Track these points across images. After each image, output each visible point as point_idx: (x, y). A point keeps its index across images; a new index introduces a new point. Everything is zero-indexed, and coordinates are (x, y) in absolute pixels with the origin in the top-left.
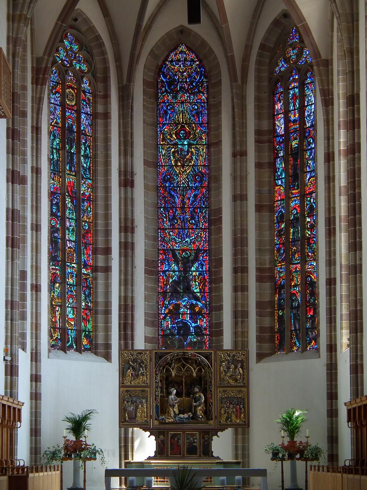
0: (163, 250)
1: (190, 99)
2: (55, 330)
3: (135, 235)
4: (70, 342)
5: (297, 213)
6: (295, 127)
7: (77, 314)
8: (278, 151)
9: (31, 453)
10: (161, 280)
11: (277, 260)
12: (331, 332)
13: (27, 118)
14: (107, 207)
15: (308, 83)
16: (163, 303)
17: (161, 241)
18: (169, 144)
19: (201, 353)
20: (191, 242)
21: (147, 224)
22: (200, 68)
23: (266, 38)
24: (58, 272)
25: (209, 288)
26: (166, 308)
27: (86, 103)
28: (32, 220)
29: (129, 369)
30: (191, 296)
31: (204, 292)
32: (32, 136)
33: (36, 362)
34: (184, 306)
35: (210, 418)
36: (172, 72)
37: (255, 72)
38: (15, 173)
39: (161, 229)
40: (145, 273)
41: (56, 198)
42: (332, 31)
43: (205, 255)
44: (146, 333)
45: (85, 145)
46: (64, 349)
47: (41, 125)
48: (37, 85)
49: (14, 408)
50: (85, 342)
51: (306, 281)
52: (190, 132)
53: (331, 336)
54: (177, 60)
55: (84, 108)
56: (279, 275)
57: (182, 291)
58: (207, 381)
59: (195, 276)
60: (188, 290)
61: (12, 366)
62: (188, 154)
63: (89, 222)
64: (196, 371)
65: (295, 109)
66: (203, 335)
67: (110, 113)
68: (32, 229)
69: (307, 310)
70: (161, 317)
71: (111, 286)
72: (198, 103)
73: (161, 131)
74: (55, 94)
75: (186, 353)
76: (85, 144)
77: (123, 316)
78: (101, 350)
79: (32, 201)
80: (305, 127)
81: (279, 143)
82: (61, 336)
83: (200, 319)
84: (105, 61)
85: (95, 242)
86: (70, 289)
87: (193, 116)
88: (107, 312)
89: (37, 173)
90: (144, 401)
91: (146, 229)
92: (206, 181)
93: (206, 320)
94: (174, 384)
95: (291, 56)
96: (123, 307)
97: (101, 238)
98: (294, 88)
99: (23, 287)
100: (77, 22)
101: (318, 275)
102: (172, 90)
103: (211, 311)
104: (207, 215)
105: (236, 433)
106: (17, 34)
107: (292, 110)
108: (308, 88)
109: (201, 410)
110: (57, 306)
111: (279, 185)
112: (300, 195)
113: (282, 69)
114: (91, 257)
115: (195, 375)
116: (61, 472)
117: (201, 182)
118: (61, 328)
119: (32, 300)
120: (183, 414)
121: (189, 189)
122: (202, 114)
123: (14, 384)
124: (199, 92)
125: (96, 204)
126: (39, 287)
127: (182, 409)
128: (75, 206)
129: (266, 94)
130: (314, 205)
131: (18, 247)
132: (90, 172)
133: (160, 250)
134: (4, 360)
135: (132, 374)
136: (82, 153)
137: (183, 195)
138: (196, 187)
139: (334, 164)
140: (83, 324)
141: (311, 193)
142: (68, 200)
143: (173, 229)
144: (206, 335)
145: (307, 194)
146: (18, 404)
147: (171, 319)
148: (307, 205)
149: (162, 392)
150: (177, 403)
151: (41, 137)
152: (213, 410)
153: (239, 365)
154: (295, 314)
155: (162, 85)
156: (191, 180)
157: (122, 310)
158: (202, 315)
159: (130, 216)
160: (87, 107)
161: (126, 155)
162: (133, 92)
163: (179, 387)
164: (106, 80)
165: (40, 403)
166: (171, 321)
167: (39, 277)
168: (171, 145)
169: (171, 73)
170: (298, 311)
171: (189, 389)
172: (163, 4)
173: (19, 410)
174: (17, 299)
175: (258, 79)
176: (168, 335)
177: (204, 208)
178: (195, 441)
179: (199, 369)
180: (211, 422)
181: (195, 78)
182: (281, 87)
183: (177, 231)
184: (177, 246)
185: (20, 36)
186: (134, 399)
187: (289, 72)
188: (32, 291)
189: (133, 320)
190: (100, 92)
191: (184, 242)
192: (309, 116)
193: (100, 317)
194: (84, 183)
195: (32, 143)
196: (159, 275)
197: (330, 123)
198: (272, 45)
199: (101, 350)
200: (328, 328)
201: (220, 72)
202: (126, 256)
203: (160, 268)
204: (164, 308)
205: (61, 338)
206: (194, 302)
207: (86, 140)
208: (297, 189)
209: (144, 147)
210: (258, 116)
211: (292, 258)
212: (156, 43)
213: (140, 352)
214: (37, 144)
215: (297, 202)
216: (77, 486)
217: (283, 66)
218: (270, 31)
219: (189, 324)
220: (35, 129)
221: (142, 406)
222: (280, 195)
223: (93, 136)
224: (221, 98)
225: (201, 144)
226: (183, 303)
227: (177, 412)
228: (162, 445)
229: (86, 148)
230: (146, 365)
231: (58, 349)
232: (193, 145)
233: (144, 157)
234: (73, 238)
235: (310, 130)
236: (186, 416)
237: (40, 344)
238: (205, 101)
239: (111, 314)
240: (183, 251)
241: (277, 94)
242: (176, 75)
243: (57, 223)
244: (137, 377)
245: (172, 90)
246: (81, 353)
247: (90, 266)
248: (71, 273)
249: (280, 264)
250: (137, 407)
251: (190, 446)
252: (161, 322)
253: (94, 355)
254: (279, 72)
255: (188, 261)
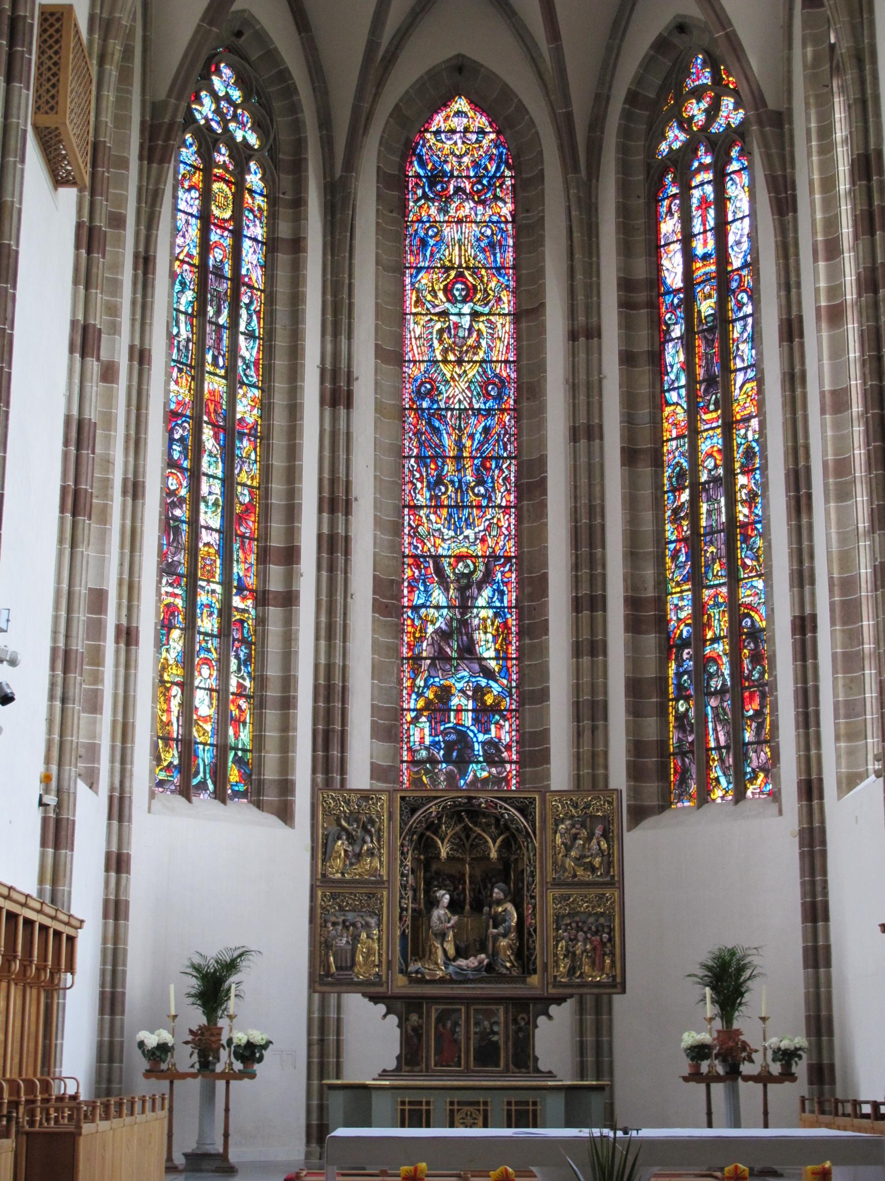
0: (415, 556)
1: (476, 214)
2: (167, 745)
3: (353, 519)
4: (201, 774)
5: (716, 467)
6: (707, 269)
7: (218, 706)
8: (668, 326)
9: (99, 1059)
10: (410, 629)
11: (672, 579)
12: (808, 748)
13: (124, 229)
14: (293, 452)
15: (734, 172)
16: (413, 685)
17: (409, 535)
18: (431, 314)
19: (510, 798)
20: (476, 539)
21: (380, 493)
22: (497, 147)
23: (639, 80)
24: (179, 602)
25: (518, 649)
26: (420, 695)
27: (255, 216)
28: (126, 472)
29: (339, 838)
30: (476, 667)
31: (506, 659)
32: (135, 277)
33: (120, 820)
34: (462, 691)
35: (531, 967)
36: (438, 156)
37: (617, 152)
38: (91, 330)
39: (409, 507)
40: (374, 611)
41: (181, 426)
42: (790, 46)
43: (507, 569)
44: (375, 755)
45: (248, 309)
46: (186, 791)
47: (155, 252)
48: (150, 162)
49: (58, 934)
50: (234, 775)
51: (740, 627)
52: (475, 287)
53: (808, 759)
54: (449, 131)
55: (248, 227)
56: (677, 614)
57: (455, 655)
58: (523, 871)
59: (484, 620)
60: (468, 651)
61: (58, 821)
62: (470, 334)
63: (251, 487)
64: (497, 844)
65: (705, 232)
66: (503, 762)
67: (305, 238)
68: (124, 493)
69: (743, 699)
70: (409, 719)
71: (297, 639)
72: (493, 222)
73: (412, 284)
74: (189, 190)
75: (475, 798)
76: (248, 306)
77: (321, 713)
78: (271, 797)
79: (127, 426)
80: (729, 269)
81: (673, 308)
82: (180, 758)
83: (497, 723)
84: (297, 126)
85: (264, 535)
86: (204, 644)
87: (483, 251)
88: (287, 703)
89: (141, 363)
90: (373, 921)
91: (377, 505)
92: (509, 397)
93: (510, 725)
94: (444, 880)
95: (693, 116)
96: (322, 691)
97: (277, 526)
98: (702, 184)
99: (96, 629)
100: (243, 38)
101: (773, 610)
102: (437, 194)
103: (521, 703)
104: (512, 475)
105: (581, 1009)
106: (111, 12)
107: (699, 234)
108: (734, 183)
109: (510, 947)
110: (173, 683)
111: (674, 404)
112: (723, 422)
113: (676, 146)
114: (254, 569)
115: (494, 855)
116: (171, 1110)
117: (499, 398)
118: (181, 740)
119: (117, 665)
120: (467, 958)
121: (474, 414)
122: (501, 246)
123: (62, 868)
124: (496, 198)
125: (268, 445)
126: (133, 634)
127: (462, 945)
128: (223, 448)
129: (642, 201)
130: (754, 444)
131: (87, 513)
132: (257, 370)
133: (408, 556)
134: (41, 804)
135: (346, 851)
136: (242, 328)
137: (460, 429)
138: (489, 411)
139: (802, 345)
140: (231, 731)
141: (747, 419)
142: (207, 432)
143: (436, 507)
144: (511, 762)
145: (738, 422)
146: (67, 924)
147: (431, 722)
148: (739, 445)
149: (415, 899)
150: (453, 927)
151: (154, 279)
152: (537, 947)
153: (598, 832)
154: (717, 707)
155: (417, 184)
156: (478, 394)
157: (321, 699)
158: (500, 712)
159: (342, 475)
160: (255, 226)
161: (336, 334)
162: (355, 194)
163: (456, 888)
164: (297, 167)
165: (126, 927)
166: (431, 728)
167: (135, 610)
168: (435, 314)
169: (435, 158)
170: (722, 701)
171: (480, 892)
172: (423, 10)
173: (71, 939)
174: (80, 645)
175: (624, 168)
176: (422, 762)
177: (506, 458)
178: (496, 1028)
179: (503, 840)
180: (534, 980)
181: (486, 168)
182: (674, 182)
183: (445, 512)
184: (446, 546)
185: (118, 15)
186: (350, 916)
187: (690, 149)
188: (117, 642)
189: (344, 723)
190: (284, 194)
191: (461, 537)
192: (738, 243)
193: (272, 715)
194: (244, 395)
195: (134, 292)
196: (405, 616)
197: (792, 250)
198: (652, 95)
199: (271, 797)
200: (802, 739)
201: (541, 153)
202: (331, 569)
203: (406, 599)
204: (414, 696)
205: (180, 764)
206: (483, 682)
207: (251, 298)
208: (716, 410)
209: (377, 318)
210: (626, 249)
211: (706, 573)
212: (407, 92)
213: (365, 796)
214: (144, 296)
215: (715, 440)
216: (208, 1147)
217: (676, 138)
218: (648, 64)
219: (471, 735)
220: (141, 261)
221: (368, 937)
222: (675, 425)
223: (268, 290)
224: (543, 211)
225: (499, 314)
226: (457, 685)
227: (451, 951)
228: (415, 1040)
229: (250, 316)
230: (380, 829)
231: (172, 792)
232: (482, 314)
233: (376, 339)
234: (216, 523)
235: (740, 276)
236: (472, 962)
237: (131, 775)
238: (510, 219)
239: (295, 707)
240: (460, 558)
241: (663, 199)
242: (446, 162)
243: (181, 485)
244: (359, 861)
245: (437, 194)
246: (224, 802)
247: (251, 591)
248: (209, 606)
249: (678, 589)
250: (356, 938)
251: (483, 1044)
252: (409, 728)
253: (254, 809)
254: (669, 153)
255: (469, 586)
